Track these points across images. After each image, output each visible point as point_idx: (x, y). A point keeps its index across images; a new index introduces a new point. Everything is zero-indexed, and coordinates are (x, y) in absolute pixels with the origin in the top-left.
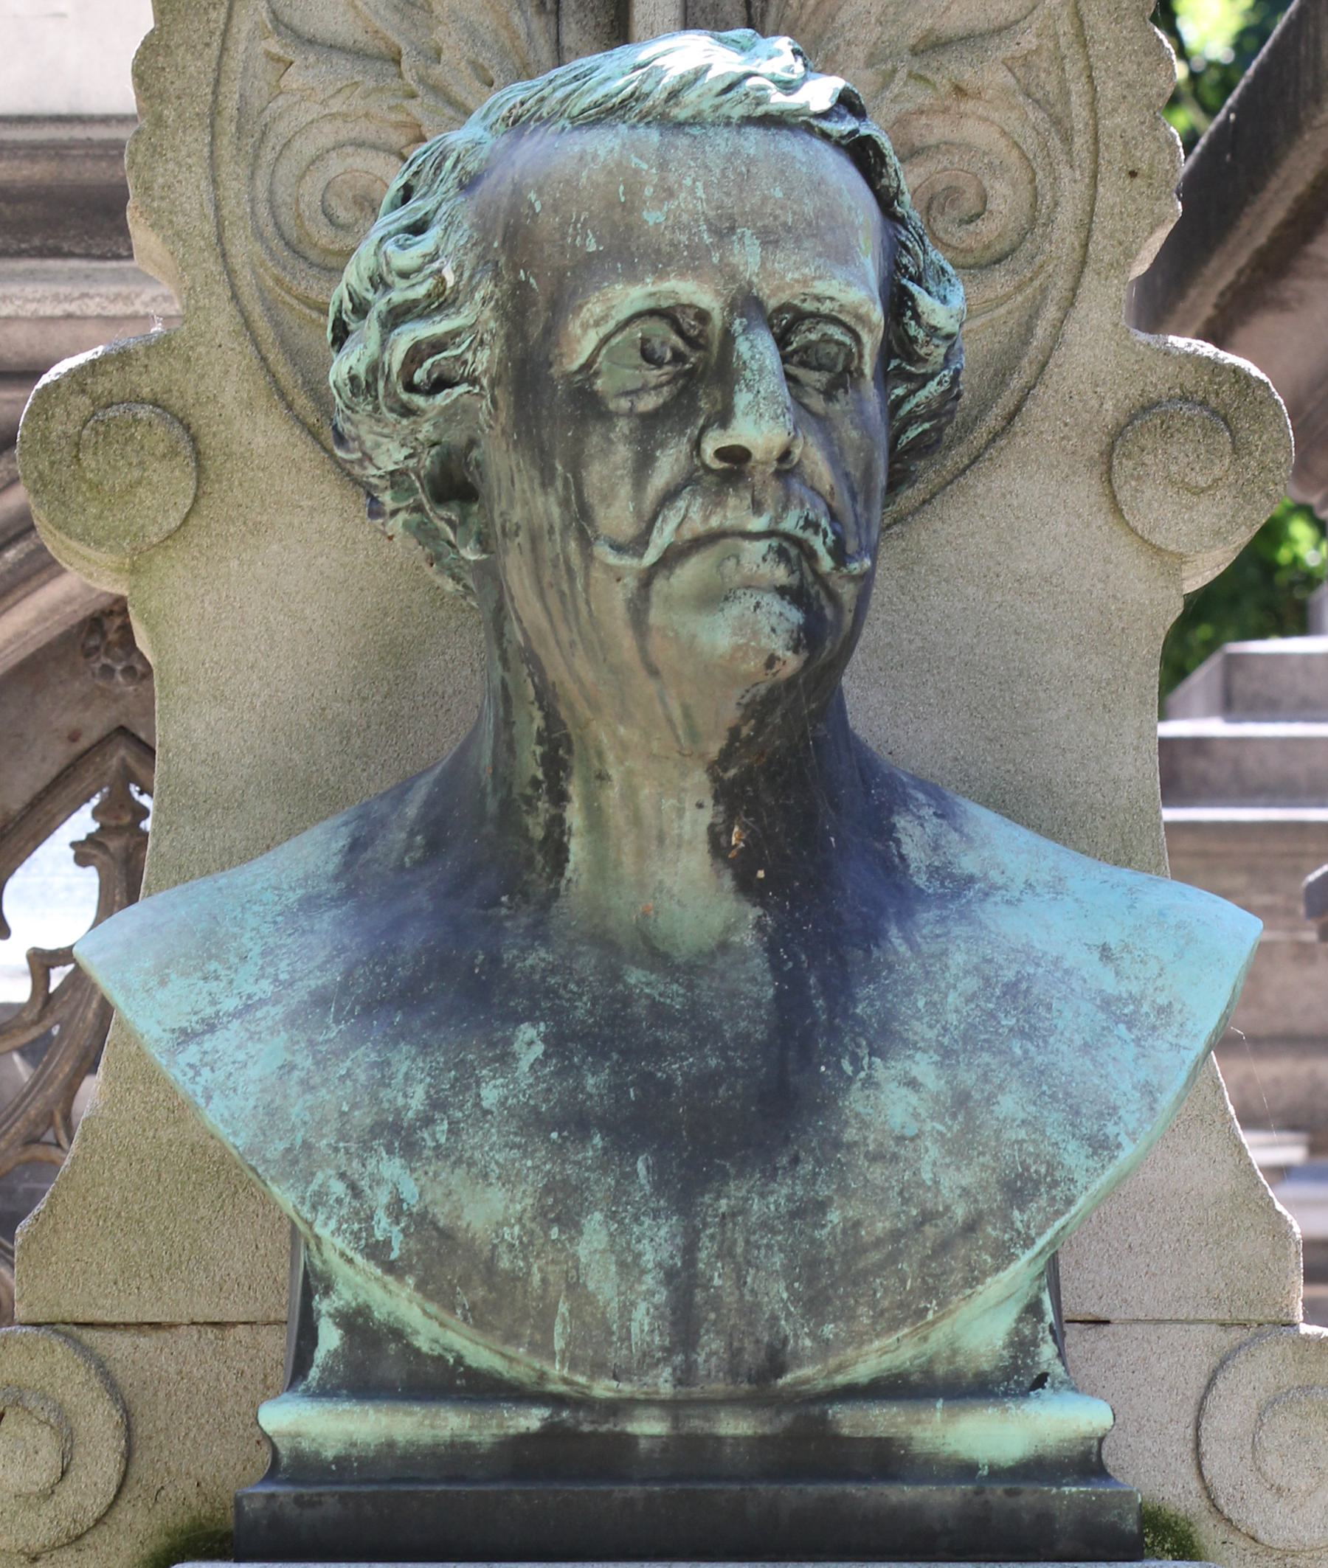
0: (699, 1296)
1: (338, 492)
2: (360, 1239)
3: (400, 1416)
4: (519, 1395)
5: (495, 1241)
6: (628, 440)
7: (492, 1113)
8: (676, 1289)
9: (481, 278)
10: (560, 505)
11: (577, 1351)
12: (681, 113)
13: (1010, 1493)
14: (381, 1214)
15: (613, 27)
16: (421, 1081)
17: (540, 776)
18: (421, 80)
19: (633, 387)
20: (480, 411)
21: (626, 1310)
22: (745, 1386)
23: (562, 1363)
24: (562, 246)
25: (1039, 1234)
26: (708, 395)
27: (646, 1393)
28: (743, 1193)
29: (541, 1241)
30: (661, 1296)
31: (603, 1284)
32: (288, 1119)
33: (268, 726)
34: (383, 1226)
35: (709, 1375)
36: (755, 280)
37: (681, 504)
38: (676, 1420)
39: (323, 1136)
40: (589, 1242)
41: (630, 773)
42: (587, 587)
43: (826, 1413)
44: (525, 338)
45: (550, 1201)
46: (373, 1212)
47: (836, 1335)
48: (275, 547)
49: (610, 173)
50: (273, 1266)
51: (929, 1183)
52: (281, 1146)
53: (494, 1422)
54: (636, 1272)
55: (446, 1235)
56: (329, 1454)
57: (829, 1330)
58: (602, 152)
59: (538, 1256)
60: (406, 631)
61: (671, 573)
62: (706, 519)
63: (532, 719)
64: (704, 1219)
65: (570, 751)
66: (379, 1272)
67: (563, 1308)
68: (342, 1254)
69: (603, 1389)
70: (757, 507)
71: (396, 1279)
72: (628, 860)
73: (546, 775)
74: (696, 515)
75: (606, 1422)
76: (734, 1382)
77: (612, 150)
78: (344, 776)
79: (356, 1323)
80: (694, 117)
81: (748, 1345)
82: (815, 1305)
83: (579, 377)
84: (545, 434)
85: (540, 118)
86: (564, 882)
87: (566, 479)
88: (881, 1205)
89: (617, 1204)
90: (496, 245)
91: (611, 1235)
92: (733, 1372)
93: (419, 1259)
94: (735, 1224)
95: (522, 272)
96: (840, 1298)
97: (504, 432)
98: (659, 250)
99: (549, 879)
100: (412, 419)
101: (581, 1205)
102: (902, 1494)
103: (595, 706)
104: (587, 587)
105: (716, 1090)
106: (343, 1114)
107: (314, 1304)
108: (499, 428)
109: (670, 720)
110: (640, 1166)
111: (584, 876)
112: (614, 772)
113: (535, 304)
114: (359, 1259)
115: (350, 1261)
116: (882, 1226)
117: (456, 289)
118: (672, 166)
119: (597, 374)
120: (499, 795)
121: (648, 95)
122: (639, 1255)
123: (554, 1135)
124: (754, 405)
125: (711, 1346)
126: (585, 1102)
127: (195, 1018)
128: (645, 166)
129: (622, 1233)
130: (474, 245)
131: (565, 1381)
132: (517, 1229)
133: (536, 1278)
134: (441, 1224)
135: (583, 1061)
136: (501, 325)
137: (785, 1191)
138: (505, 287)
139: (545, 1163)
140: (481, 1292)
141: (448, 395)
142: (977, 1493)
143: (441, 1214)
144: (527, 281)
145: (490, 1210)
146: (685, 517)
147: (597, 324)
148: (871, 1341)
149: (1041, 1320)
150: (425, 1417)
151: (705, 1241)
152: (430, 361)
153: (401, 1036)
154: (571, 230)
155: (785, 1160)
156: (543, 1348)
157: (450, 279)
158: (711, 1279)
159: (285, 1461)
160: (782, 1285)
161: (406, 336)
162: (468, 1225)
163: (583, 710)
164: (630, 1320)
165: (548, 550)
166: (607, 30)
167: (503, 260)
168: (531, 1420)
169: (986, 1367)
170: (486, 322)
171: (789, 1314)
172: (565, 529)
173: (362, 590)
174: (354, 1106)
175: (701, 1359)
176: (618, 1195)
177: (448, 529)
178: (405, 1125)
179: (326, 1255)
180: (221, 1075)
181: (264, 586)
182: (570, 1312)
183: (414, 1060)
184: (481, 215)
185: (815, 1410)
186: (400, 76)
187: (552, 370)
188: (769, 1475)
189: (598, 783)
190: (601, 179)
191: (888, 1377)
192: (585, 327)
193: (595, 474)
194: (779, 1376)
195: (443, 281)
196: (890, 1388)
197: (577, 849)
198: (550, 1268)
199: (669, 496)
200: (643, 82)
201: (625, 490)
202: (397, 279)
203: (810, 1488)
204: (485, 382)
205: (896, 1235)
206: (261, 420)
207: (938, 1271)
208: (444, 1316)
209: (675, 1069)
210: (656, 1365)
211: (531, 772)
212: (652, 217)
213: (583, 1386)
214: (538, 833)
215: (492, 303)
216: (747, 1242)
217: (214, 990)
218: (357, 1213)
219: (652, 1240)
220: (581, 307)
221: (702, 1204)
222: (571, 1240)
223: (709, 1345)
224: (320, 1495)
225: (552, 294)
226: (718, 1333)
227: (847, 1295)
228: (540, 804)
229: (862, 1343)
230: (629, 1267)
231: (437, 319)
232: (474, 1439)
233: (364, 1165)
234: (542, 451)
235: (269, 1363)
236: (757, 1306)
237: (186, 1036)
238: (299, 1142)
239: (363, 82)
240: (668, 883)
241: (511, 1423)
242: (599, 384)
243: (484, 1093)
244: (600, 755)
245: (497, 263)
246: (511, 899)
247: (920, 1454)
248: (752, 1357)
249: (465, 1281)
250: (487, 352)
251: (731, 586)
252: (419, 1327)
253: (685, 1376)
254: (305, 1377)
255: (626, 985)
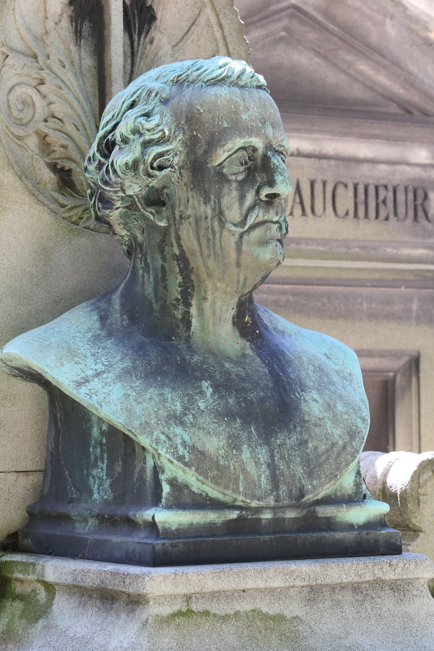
0: (277, 472)
1: (28, 198)
2: (175, 455)
3: (196, 515)
4: (232, 507)
5: (217, 455)
6: (236, 189)
7: (204, 411)
8: (271, 470)
9: (179, 133)
10: (212, 210)
11: (247, 492)
12: (242, 83)
13: (368, 534)
14: (179, 446)
15: (94, 52)
16: (177, 400)
17: (180, 297)
18: (45, 64)
19: (235, 172)
20: (172, 178)
21: (259, 477)
22: (294, 502)
23: (243, 495)
24: (214, 124)
25: (360, 449)
26: (260, 176)
27: (267, 505)
28: (283, 438)
29: (231, 455)
30: (267, 473)
31: (251, 468)
32: (136, 413)
33: (9, 274)
34: (181, 450)
35: (284, 498)
36: (272, 139)
37: (256, 211)
38: (275, 513)
39: (151, 419)
40: (245, 455)
41: (215, 298)
42: (221, 237)
43: (315, 509)
44: (195, 154)
45: (231, 441)
46: (177, 445)
47: (317, 484)
48: (10, 215)
49: (228, 101)
50: (11, 453)
51: (331, 433)
52: (138, 423)
53: (224, 516)
54: (259, 465)
55: (202, 453)
56: (174, 528)
57: (315, 482)
58: (223, 94)
59: (231, 460)
60: (48, 244)
61: (249, 234)
62: (264, 216)
63: (177, 279)
64: (274, 447)
65: (193, 290)
66: (182, 466)
67: (241, 477)
68: (169, 460)
69: (254, 504)
70: (277, 214)
71: (189, 468)
72: (211, 326)
73: (181, 297)
74: (261, 215)
75: (255, 515)
76: (291, 500)
77: (226, 94)
78: (31, 291)
79: (173, 482)
80: (245, 85)
81: (294, 488)
82: (310, 474)
83: (217, 168)
84: (207, 186)
85: (189, 81)
86: (191, 333)
87: (215, 202)
88: (321, 440)
89: (250, 442)
90: (182, 122)
91: (251, 452)
92: (290, 497)
93: (195, 461)
94: (283, 448)
95: (195, 132)
96: (316, 472)
97: (185, 184)
98: (248, 128)
99: (186, 332)
100: (152, 178)
101: (240, 442)
102: (339, 535)
103: (210, 275)
104: (221, 237)
105: (266, 403)
106: (155, 412)
107: (159, 477)
108: (183, 183)
109: (238, 281)
110: (252, 429)
111: (198, 331)
112: (209, 297)
113: (200, 143)
114: (175, 462)
115: (172, 462)
116: (323, 448)
117: (169, 136)
118: (246, 100)
119: (223, 167)
120: (159, 303)
121: (231, 76)
122: (259, 459)
123: (226, 419)
124: (283, 181)
125: (283, 488)
126: (231, 407)
127: (79, 377)
128: (239, 100)
129: (253, 452)
130: (173, 122)
131: (243, 501)
132: (223, 450)
133: (232, 467)
134: (200, 450)
135: (225, 393)
136: (185, 149)
137: (295, 437)
138: (187, 136)
139: (226, 428)
140: (216, 472)
141: (165, 171)
142: (359, 534)
143: (199, 445)
144: (197, 135)
145: (214, 444)
146: (257, 215)
147: (229, 151)
148: (325, 486)
149: (361, 477)
150: (204, 515)
151: (276, 454)
152: (159, 159)
153: (163, 385)
154: (217, 119)
155: (292, 427)
156: (236, 491)
157: (167, 133)
158: (280, 466)
159: (161, 531)
160: (301, 468)
161: (155, 150)
162: (208, 450)
163: (204, 276)
164: (261, 481)
165: (203, 224)
166: (92, 52)
167: (186, 127)
168: (234, 515)
169: (350, 493)
170: (178, 148)
171: (304, 478)
172: (213, 218)
173: (36, 230)
174: (158, 409)
175: (281, 493)
176: (249, 438)
177: (151, 215)
178: (178, 415)
179: (161, 460)
180: (101, 397)
181: (7, 228)
182: (244, 478)
183: (172, 393)
184: (174, 112)
185: (312, 509)
186: (37, 62)
187: (208, 165)
188: (299, 530)
189: (203, 301)
190: (225, 103)
191: (326, 497)
192: (224, 152)
193: (225, 200)
194: (303, 498)
195: (164, 133)
196: (327, 501)
197: (195, 322)
198: (236, 464)
199: (251, 209)
200: (228, 72)
201: (236, 206)
202: (146, 132)
203: (314, 535)
204: (176, 167)
205: (327, 451)
206: (6, 173)
207: (339, 462)
208: (205, 480)
209: (252, 396)
210: (269, 495)
211: (176, 296)
212: (244, 117)
213: (249, 503)
214: (180, 316)
215: (181, 142)
216: (288, 454)
217: (81, 368)
218: (172, 446)
219: (261, 454)
220: (224, 145)
221: (272, 441)
222: (240, 454)
223: (282, 488)
224: (178, 543)
225: (208, 140)
226: (284, 484)
227: (318, 471)
228: (179, 307)
229: (323, 487)
230: (257, 463)
231: (164, 146)
232: (216, 522)
233: (169, 429)
234: (205, 192)
235: (10, 485)
236: (294, 475)
237: (79, 384)
238: (144, 422)
239: (27, 64)
240: (221, 334)
241: (228, 516)
242: (225, 171)
243: (199, 404)
244: (205, 291)
245: (184, 128)
246: (176, 338)
247: (338, 522)
248: (295, 492)
249: (210, 468)
250: (178, 158)
251: (267, 239)
252: (193, 484)
253: (277, 499)
254: (161, 502)
255: (226, 368)
